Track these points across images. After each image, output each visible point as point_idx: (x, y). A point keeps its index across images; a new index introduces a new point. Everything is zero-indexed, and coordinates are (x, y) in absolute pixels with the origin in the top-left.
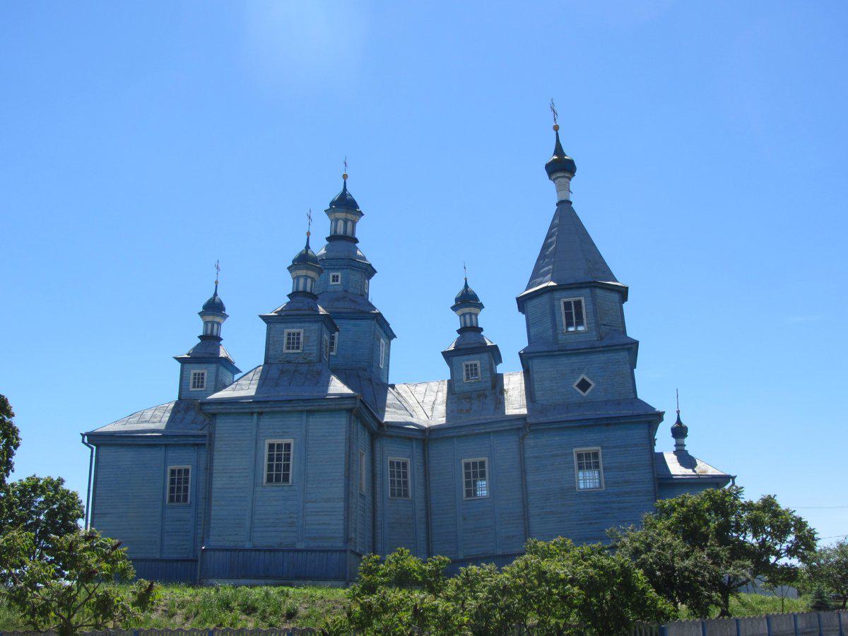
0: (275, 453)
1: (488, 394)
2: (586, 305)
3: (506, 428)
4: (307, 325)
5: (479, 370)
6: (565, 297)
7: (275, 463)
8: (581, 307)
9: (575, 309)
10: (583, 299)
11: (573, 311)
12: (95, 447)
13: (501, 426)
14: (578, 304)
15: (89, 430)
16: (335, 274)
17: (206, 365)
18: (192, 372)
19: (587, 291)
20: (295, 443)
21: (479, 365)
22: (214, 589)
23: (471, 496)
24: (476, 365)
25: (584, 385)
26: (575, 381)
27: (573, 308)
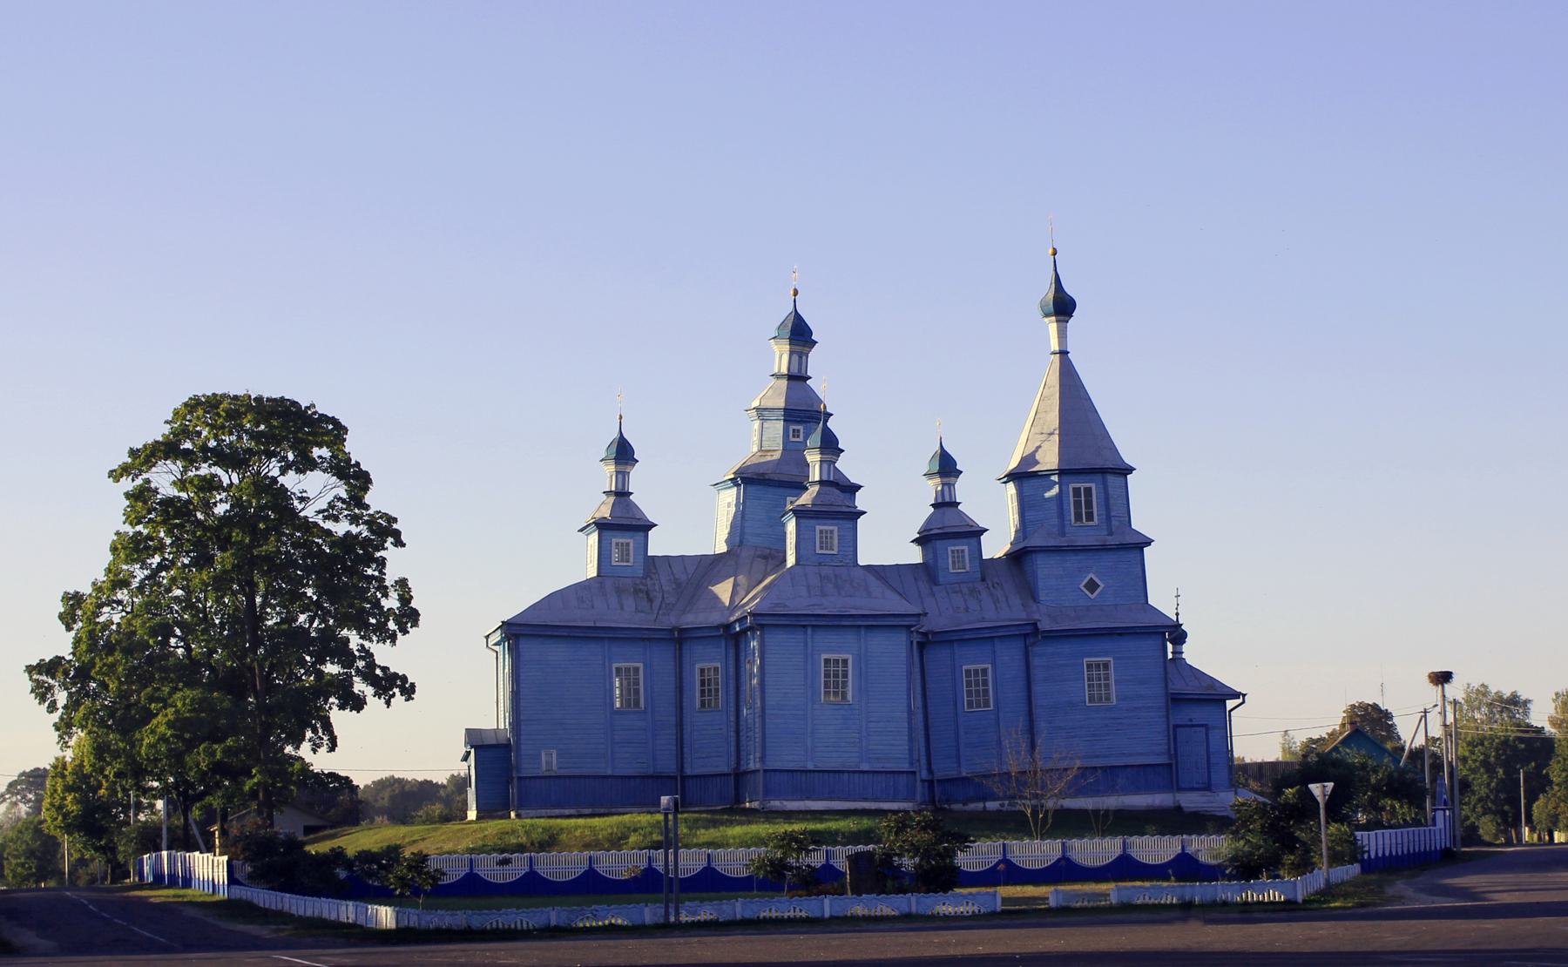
4: (841, 522)
7: (981, 688)
8: (1091, 496)
9: (1085, 497)
10: (1093, 486)
11: (1083, 499)
14: (1088, 491)
16: (796, 427)
19: (1099, 477)
23: (972, 708)
25: (1092, 586)
26: (1083, 581)
27: (1083, 496)
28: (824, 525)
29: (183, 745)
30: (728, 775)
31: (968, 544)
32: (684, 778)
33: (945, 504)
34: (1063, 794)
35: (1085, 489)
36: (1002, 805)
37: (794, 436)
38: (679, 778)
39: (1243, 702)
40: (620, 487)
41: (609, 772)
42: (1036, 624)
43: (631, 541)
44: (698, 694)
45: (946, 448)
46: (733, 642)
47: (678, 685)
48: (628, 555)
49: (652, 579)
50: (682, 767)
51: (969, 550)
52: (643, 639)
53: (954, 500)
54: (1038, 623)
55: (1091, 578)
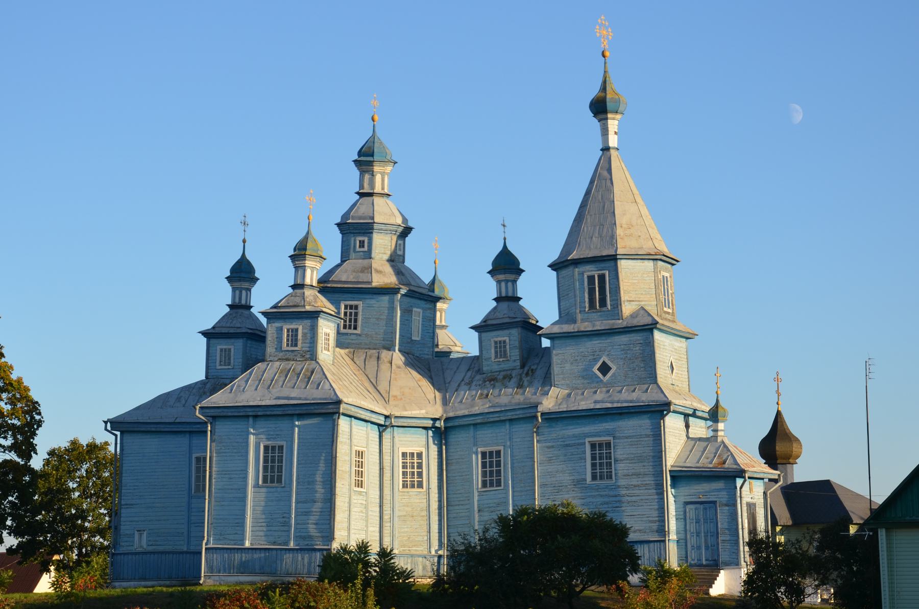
0: (270, 455)
1: (513, 375)
2: (609, 280)
3: (521, 416)
5: (508, 347)
6: (589, 271)
7: (488, 469)
12: (118, 433)
13: (516, 415)
15: (111, 416)
17: (233, 340)
18: (219, 347)
20: (287, 445)
21: (507, 341)
22: (297, 602)
24: (504, 342)
29: (451, 592)
33: (507, 299)
35: (599, 276)
40: (237, 300)
41: (185, 549)
43: (232, 347)
45: (510, 248)
48: (229, 359)
55: (604, 362)
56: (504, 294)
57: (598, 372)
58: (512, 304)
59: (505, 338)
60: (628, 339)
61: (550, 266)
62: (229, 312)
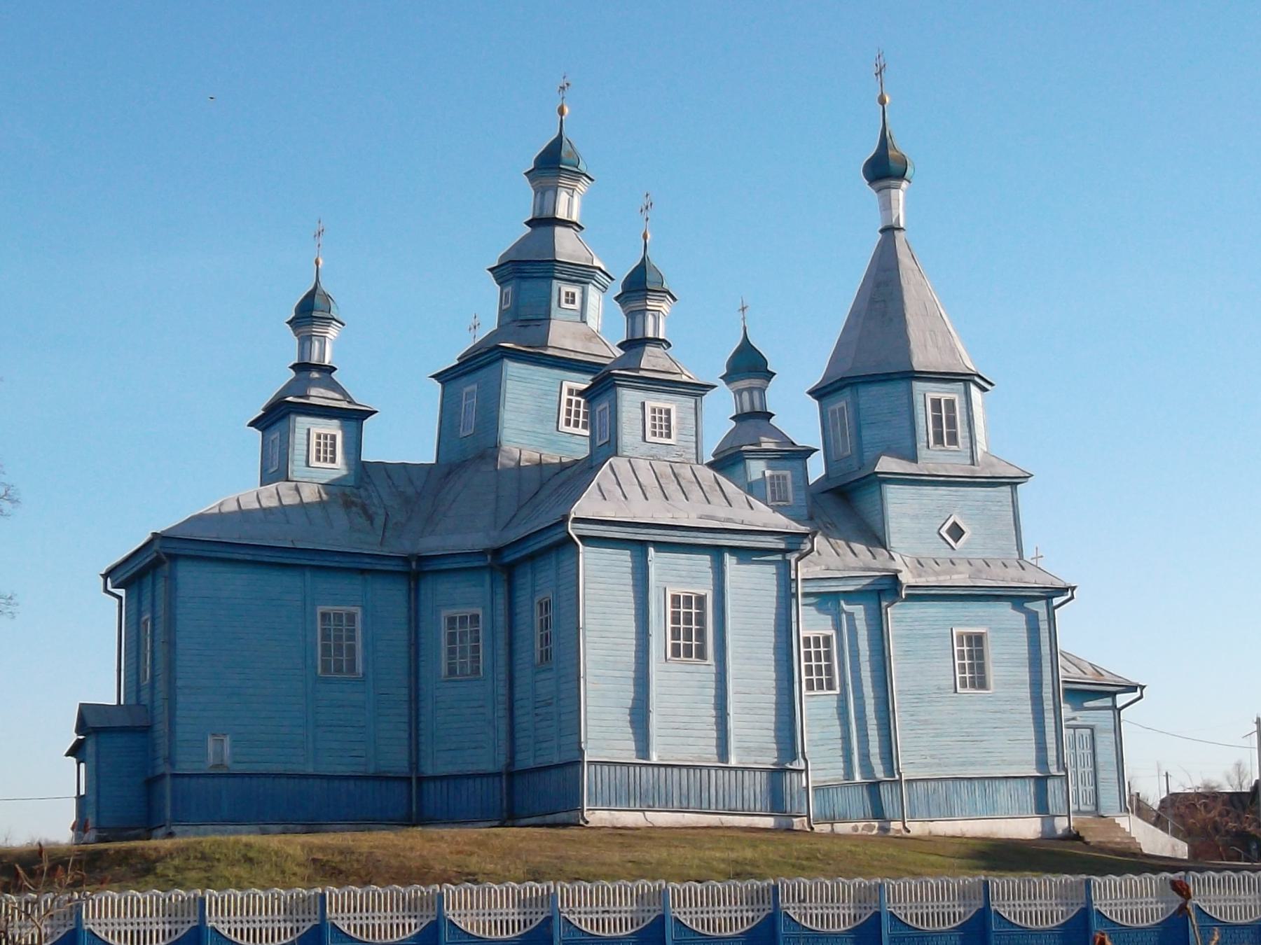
28: (658, 400)
30: (499, 774)
31: (791, 469)
32: (421, 780)
34: (1171, 823)
36: (855, 829)
37: (567, 301)
38: (414, 781)
39: (1141, 697)
42: (896, 577)
44: (444, 654)
46: (505, 577)
47: (413, 642)
49: (366, 490)
50: (417, 763)
51: (792, 476)
52: (363, 571)
53: (764, 410)
54: (899, 575)
56: (747, 408)
57: (951, 523)
58: (762, 423)
59: (353, 609)
60: (983, 494)
61: (810, 393)
62: (295, 378)
